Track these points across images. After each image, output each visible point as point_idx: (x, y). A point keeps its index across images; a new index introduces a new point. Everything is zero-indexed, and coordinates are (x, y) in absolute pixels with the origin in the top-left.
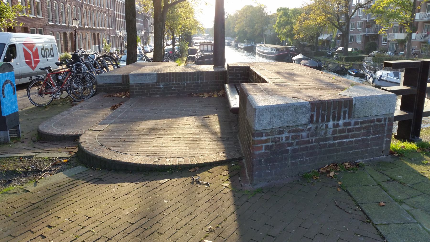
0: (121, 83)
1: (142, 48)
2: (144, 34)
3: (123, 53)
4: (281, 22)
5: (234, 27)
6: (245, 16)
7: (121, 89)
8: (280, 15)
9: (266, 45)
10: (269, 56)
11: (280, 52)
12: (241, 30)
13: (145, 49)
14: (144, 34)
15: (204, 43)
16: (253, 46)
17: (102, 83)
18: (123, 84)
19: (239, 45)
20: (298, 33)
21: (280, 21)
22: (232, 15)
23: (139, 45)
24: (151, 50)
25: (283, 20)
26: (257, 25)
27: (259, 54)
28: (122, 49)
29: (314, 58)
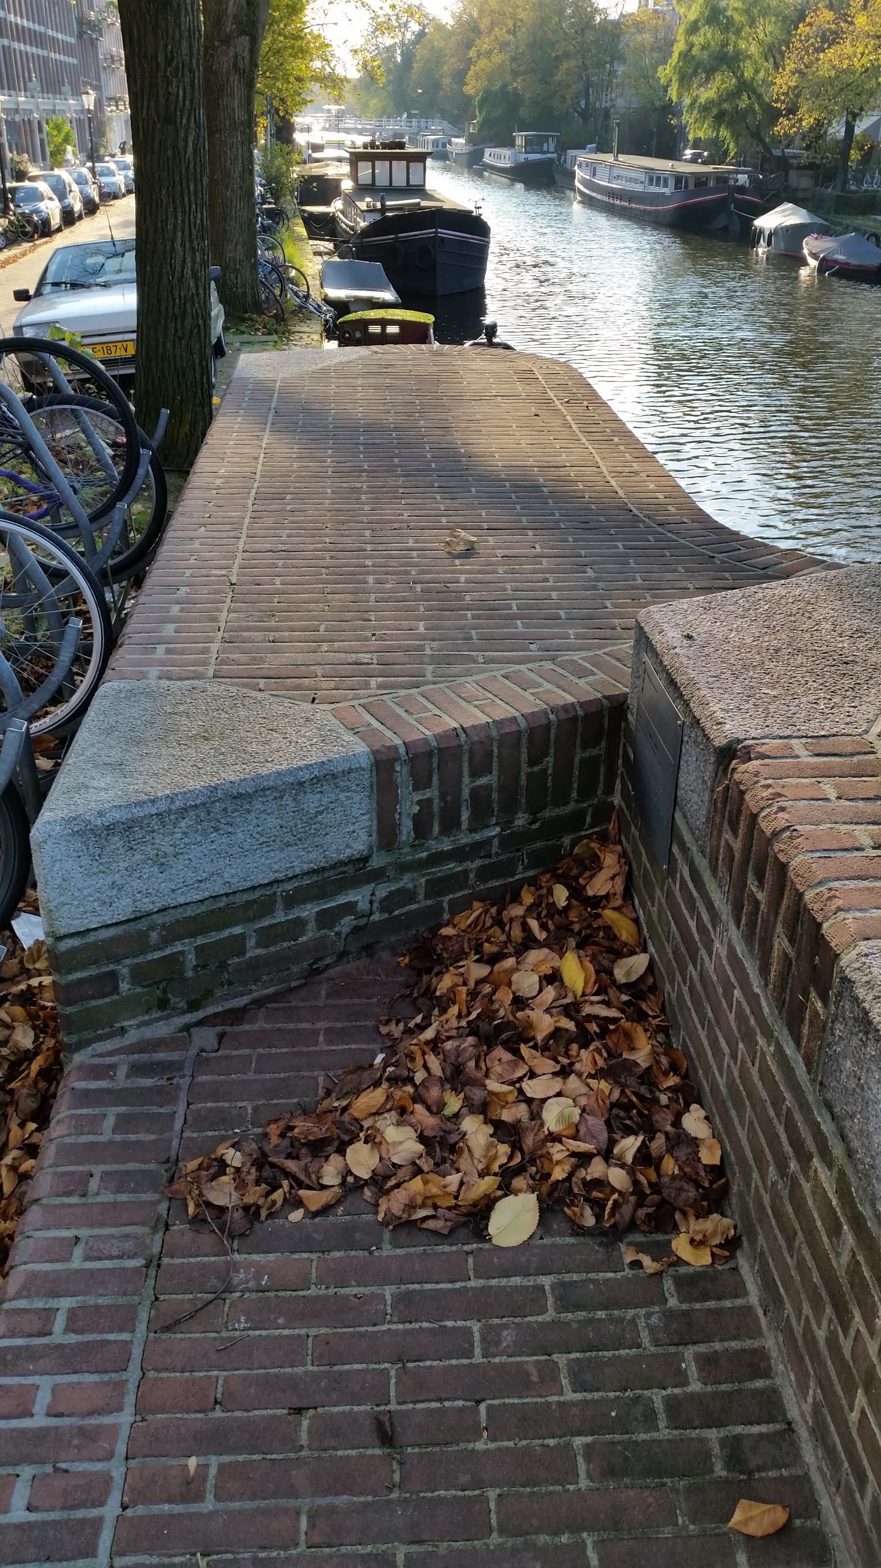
0: (365, 860)
1: (89, 176)
2: (92, 108)
3: (12, 206)
4: (695, 51)
5: (460, 76)
6: (510, 23)
7: (356, 930)
8: (692, 16)
9: (621, 157)
10: (642, 207)
11: (694, 195)
12: (494, 88)
13: (104, 180)
14: (92, 108)
15: (370, 150)
16: (550, 161)
17: (123, 909)
18: (376, 862)
19: (487, 155)
20: (792, 110)
21: (691, 46)
22: (447, 20)
23: (67, 161)
24: (126, 186)
25: (702, 40)
26: (564, 66)
27: (591, 198)
28: (8, 185)
29: (840, 224)
